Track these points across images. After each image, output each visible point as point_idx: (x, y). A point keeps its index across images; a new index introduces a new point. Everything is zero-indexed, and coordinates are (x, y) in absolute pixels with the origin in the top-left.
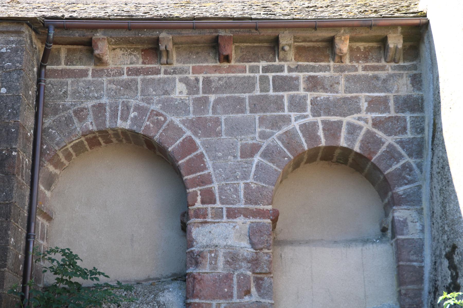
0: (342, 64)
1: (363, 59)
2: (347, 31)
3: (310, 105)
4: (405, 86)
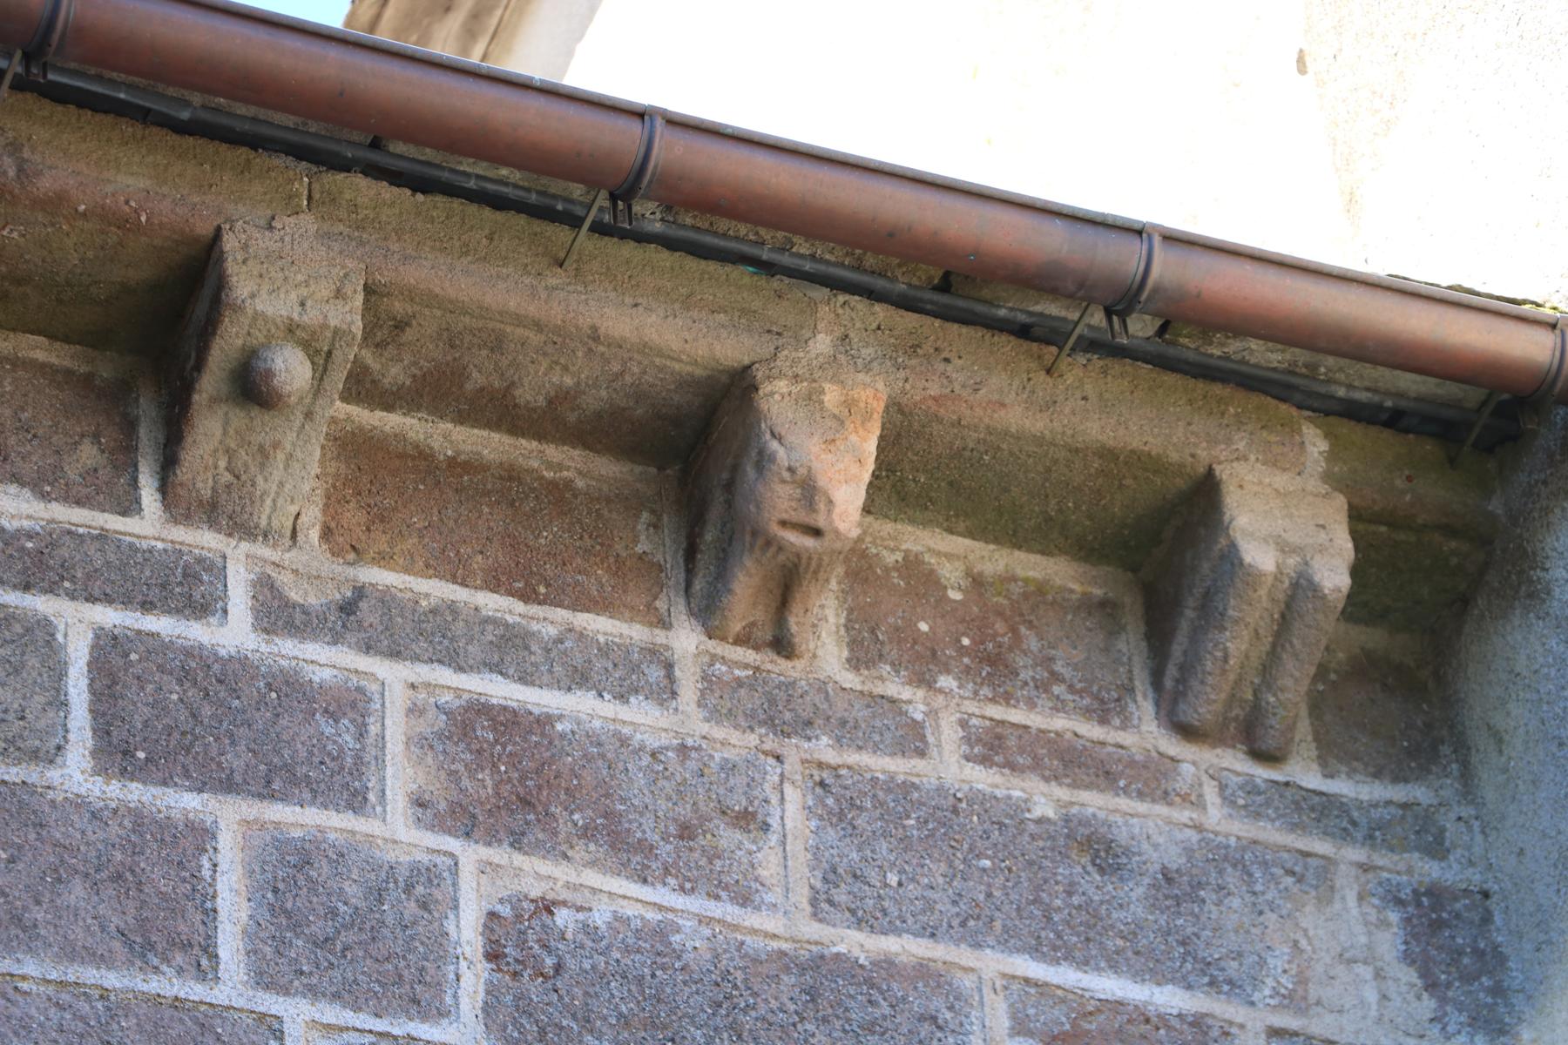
0: (783, 664)
1: (968, 670)
2: (867, 352)
3: (484, 967)
4: (1366, 972)
